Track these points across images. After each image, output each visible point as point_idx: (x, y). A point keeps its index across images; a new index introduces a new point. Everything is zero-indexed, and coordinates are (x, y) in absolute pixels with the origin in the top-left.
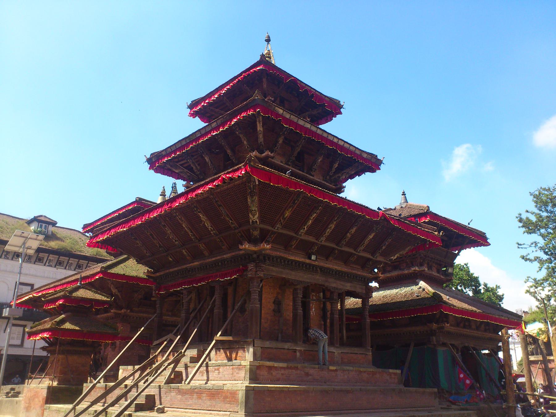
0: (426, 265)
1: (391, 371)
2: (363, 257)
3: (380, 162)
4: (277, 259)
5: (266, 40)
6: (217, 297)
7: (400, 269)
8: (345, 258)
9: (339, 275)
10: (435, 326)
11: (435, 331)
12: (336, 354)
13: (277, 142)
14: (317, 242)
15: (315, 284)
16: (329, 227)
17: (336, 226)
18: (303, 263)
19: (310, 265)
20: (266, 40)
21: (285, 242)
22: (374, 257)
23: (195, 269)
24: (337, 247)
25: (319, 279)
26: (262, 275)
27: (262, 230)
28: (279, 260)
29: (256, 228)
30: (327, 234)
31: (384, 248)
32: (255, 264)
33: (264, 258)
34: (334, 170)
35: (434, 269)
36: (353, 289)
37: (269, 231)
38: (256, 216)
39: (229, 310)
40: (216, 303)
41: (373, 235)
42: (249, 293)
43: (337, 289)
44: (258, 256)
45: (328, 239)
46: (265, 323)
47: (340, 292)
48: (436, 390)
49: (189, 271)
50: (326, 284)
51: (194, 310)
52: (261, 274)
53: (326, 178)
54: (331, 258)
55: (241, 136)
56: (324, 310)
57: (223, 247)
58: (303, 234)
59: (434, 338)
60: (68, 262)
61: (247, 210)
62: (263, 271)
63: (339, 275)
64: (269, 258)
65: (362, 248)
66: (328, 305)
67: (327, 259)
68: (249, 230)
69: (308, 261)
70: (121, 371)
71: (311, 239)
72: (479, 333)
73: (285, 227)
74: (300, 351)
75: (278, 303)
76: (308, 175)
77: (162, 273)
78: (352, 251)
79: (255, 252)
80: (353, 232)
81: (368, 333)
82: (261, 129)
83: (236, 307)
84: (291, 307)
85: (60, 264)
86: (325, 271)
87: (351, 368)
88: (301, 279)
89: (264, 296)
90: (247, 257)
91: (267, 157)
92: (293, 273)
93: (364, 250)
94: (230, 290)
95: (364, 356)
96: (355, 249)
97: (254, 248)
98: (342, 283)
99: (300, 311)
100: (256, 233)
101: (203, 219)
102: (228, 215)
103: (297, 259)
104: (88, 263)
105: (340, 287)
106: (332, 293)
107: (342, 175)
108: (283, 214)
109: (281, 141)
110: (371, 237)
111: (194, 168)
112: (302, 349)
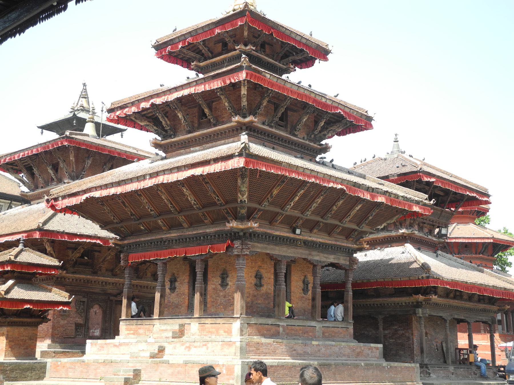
0: (416, 226)
1: (372, 345)
3: (370, 119)
4: (262, 236)
7: (388, 231)
8: (329, 230)
10: (421, 297)
11: (421, 302)
12: (317, 328)
14: (302, 216)
16: (316, 201)
17: (323, 200)
18: (288, 238)
21: (271, 219)
22: (359, 227)
23: (173, 241)
26: (248, 253)
27: (249, 208)
28: (264, 236)
29: (243, 207)
30: (313, 208)
31: (370, 218)
32: (241, 241)
34: (319, 128)
36: (336, 262)
38: (245, 196)
41: (359, 207)
43: (320, 262)
44: (245, 234)
46: (248, 297)
49: (165, 242)
50: (309, 258)
53: (310, 137)
54: (315, 231)
55: (222, 97)
57: (206, 221)
58: (289, 210)
59: (420, 310)
62: (249, 249)
65: (349, 219)
67: (311, 231)
68: (236, 208)
69: (292, 235)
72: (472, 304)
73: (271, 204)
74: (283, 326)
76: (292, 137)
77: (132, 241)
78: (337, 222)
79: (242, 230)
80: (339, 205)
82: (246, 93)
84: (273, 280)
86: (307, 244)
87: (333, 343)
88: (284, 254)
90: (233, 234)
91: (252, 122)
92: (277, 248)
93: (350, 221)
95: (345, 329)
97: (241, 227)
98: (326, 255)
100: (244, 211)
101: (187, 194)
102: (214, 192)
103: (282, 234)
105: (324, 259)
107: (328, 133)
108: (271, 192)
109: (265, 103)
110: (358, 208)
111: (163, 122)
112: (285, 324)
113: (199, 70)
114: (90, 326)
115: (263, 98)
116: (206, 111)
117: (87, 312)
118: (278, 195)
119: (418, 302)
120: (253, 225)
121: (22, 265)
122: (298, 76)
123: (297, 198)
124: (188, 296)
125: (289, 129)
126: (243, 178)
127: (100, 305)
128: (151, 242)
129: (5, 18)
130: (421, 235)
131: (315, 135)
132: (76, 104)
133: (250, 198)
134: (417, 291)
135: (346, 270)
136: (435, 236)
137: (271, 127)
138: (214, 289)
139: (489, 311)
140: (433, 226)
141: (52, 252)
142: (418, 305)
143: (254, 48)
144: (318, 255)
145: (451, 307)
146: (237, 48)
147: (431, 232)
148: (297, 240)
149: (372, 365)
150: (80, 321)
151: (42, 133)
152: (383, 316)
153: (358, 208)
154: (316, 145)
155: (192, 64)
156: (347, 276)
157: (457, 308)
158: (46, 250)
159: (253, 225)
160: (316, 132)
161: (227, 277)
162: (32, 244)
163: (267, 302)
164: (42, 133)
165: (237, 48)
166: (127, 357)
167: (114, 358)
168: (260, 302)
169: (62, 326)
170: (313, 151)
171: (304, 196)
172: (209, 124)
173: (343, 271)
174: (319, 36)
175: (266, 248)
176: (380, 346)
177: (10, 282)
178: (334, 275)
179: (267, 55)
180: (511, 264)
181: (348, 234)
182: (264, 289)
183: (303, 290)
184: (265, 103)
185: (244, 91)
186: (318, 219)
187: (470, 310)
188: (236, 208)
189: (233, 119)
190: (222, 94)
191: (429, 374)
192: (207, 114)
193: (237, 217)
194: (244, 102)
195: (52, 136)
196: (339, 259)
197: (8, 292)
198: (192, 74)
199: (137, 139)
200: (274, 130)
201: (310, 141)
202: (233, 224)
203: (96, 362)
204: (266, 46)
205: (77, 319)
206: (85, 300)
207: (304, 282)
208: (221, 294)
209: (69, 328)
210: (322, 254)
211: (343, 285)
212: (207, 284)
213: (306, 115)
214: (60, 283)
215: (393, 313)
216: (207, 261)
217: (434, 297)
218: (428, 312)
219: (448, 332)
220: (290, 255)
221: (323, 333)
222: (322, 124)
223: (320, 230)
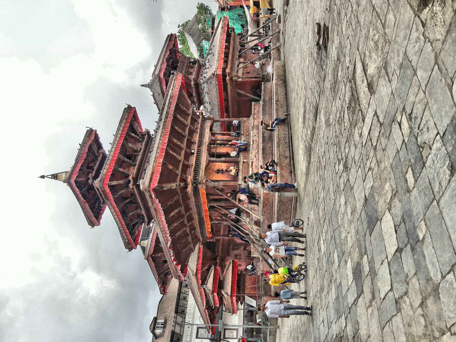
2: (191, 121)
6: (215, 204)
7: (193, 92)
9: (202, 136)
10: (228, 78)
13: (122, 172)
15: (207, 150)
19: (197, 153)
21: (186, 167)
25: (204, 149)
27: (180, 181)
29: (180, 185)
31: (185, 109)
33: (195, 180)
34: (136, 136)
35: (192, 70)
36: (209, 128)
37: (181, 178)
39: (222, 197)
40: (219, 205)
42: (214, 187)
44: (194, 183)
48: (263, 83)
50: (207, 144)
51: (221, 217)
52: (204, 181)
55: (119, 194)
56: (220, 144)
60: (182, 306)
61: (170, 190)
64: (195, 177)
65: (186, 122)
66: (218, 142)
69: (195, 155)
70: (254, 256)
71: (183, 153)
74: (243, 159)
75: (218, 171)
79: (192, 185)
83: (221, 194)
85: (183, 311)
88: (205, 159)
89: (215, 179)
91: (133, 178)
92: (202, 163)
94: (211, 197)
96: (187, 126)
99: (223, 159)
100: (182, 184)
104: (182, 293)
106: (212, 140)
108: (171, 170)
109: (121, 170)
111: (136, 221)
112: (242, 158)
115: (119, 171)
118: (172, 165)
119: (230, 80)
120: (190, 179)
121: (214, 287)
122: (107, 147)
126: (163, 188)
130: (194, 74)
133: (174, 181)
134: (224, 80)
139: (234, 37)
142: (231, 79)
143: (91, 174)
145: (232, 60)
156: (217, 121)
157: (233, 57)
159: (190, 179)
162: (204, 281)
170: (148, 138)
172: (135, 198)
173: (215, 124)
174: (80, 137)
176: (253, 103)
177: (223, 292)
178: (217, 128)
179: (95, 165)
181: (194, 121)
184: (121, 170)
185: (114, 183)
186: (186, 140)
187: (234, 48)
188: (180, 188)
193: (186, 187)
194: (121, 182)
196: (208, 126)
197: (227, 294)
202: (190, 189)
206: (232, 246)
210: (205, 136)
211: (223, 123)
214: (223, 267)
217: (228, 71)
220: (206, 155)
221: (247, 136)
222: (133, 135)
223: (192, 138)
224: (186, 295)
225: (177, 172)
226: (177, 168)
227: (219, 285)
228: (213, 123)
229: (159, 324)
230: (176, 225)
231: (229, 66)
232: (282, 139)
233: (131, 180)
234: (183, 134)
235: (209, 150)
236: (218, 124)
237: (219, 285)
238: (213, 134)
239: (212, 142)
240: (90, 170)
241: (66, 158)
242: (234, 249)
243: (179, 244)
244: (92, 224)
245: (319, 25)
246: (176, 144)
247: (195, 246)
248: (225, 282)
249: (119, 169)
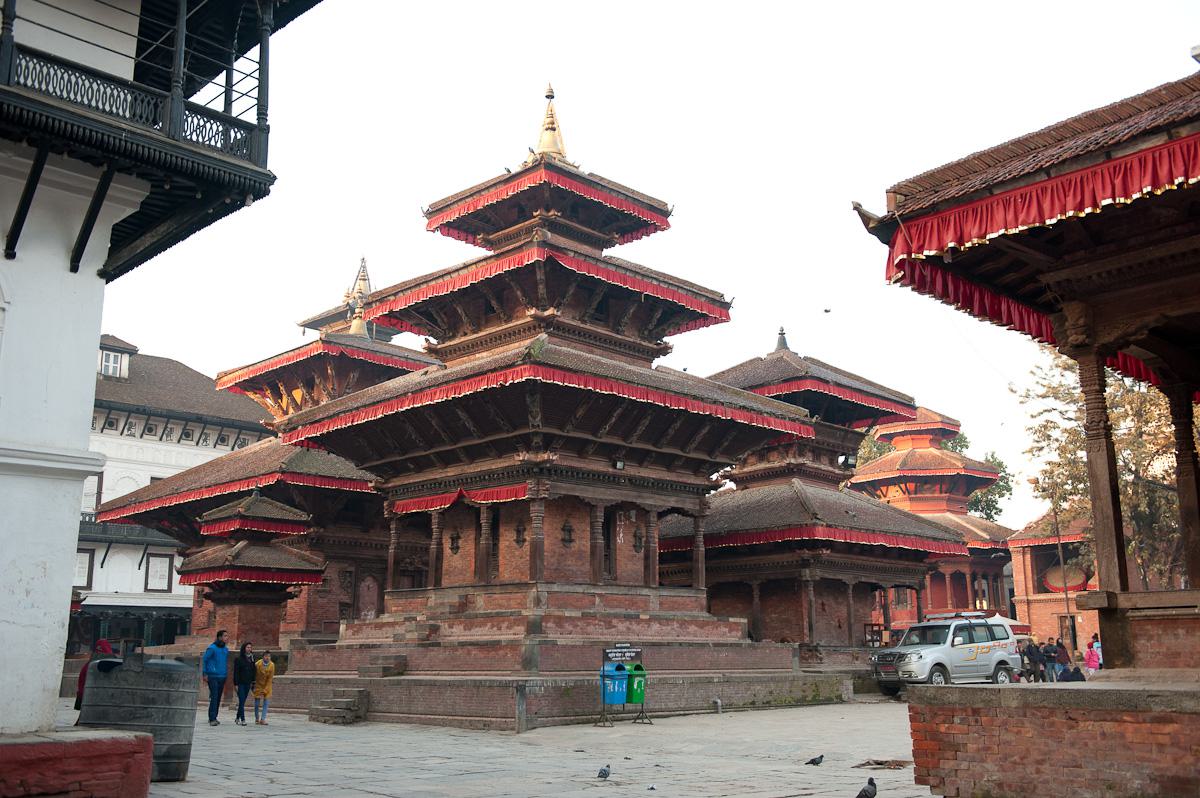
1: (731, 620)
4: (567, 472)
5: (547, 97)
9: (659, 486)
10: (806, 553)
18: (605, 474)
19: (614, 476)
20: (547, 97)
24: (655, 449)
27: (545, 435)
28: (570, 473)
31: (726, 444)
34: (655, 321)
36: (680, 506)
37: (554, 435)
43: (655, 506)
45: (640, 439)
46: (552, 557)
47: (660, 510)
50: (638, 501)
54: (646, 463)
55: (512, 284)
59: (807, 571)
63: (659, 486)
81: (702, 566)
82: (543, 277)
84: (589, 533)
85: (150, 430)
86: (635, 483)
88: (601, 497)
98: (663, 497)
99: (601, 541)
105: (660, 503)
107: (668, 327)
111: (439, 320)
113: (488, 244)
114: (361, 605)
116: (494, 303)
117: (355, 587)
122: (628, 253)
123: (614, 420)
124: (475, 558)
125: (611, 324)
126: (532, 395)
127: (374, 578)
128: (422, 484)
129: (153, 233)
131: (650, 331)
132: (351, 290)
133: (546, 421)
135: (695, 517)
136: (839, 468)
137: (584, 322)
138: (508, 547)
140: (836, 452)
141: (303, 503)
144: (652, 498)
146: (535, 214)
147: (833, 462)
148: (620, 477)
149: (594, 616)
150: (346, 599)
151: (304, 332)
152: (760, 581)
153: (705, 431)
154: (651, 345)
155: (478, 237)
156: (696, 527)
158: (293, 500)
160: (650, 327)
161: (525, 529)
163: (580, 563)
164: (304, 332)
165: (535, 214)
166: (390, 640)
167: (375, 641)
168: (570, 562)
169: (322, 607)
171: (622, 417)
175: (573, 489)
177: (241, 544)
180: (1001, 511)
182: (575, 546)
183: (634, 546)
185: (540, 275)
187: (884, 570)
189: (528, 313)
190: (512, 280)
191: (821, 659)
192: (496, 307)
195: (314, 335)
196: (684, 502)
198: (481, 252)
199: (411, 341)
200: (588, 326)
201: (643, 339)
203: (349, 647)
204: (580, 209)
205: (342, 596)
206: (352, 569)
207: (635, 536)
208: (517, 553)
209: (332, 609)
211: (690, 540)
212: (498, 539)
213: (633, 304)
215: (772, 577)
216: (498, 510)
218: (819, 573)
219: (851, 602)
224: (160, 433)
225: (569, 427)
226: (578, 428)
227: (259, 534)
228: (691, 516)
229: (115, 362)
230: (433, 423)
231: (837, 557)
232: (656, 693)
233: (547, 313)
234: (664, 441)
235: (625, 506)
236: (688, 530)
237: (259, 534)
238: (661, 515)
239: (643, 512)
240: (568, 213)
241: (601, 155)
242: (343, 573)
243: (382, 431)
244: (433, 212)
245: (547, 129)
246: (638, 424)
247: (370, 469)
248: (267, 549)
249: (574, 285)
